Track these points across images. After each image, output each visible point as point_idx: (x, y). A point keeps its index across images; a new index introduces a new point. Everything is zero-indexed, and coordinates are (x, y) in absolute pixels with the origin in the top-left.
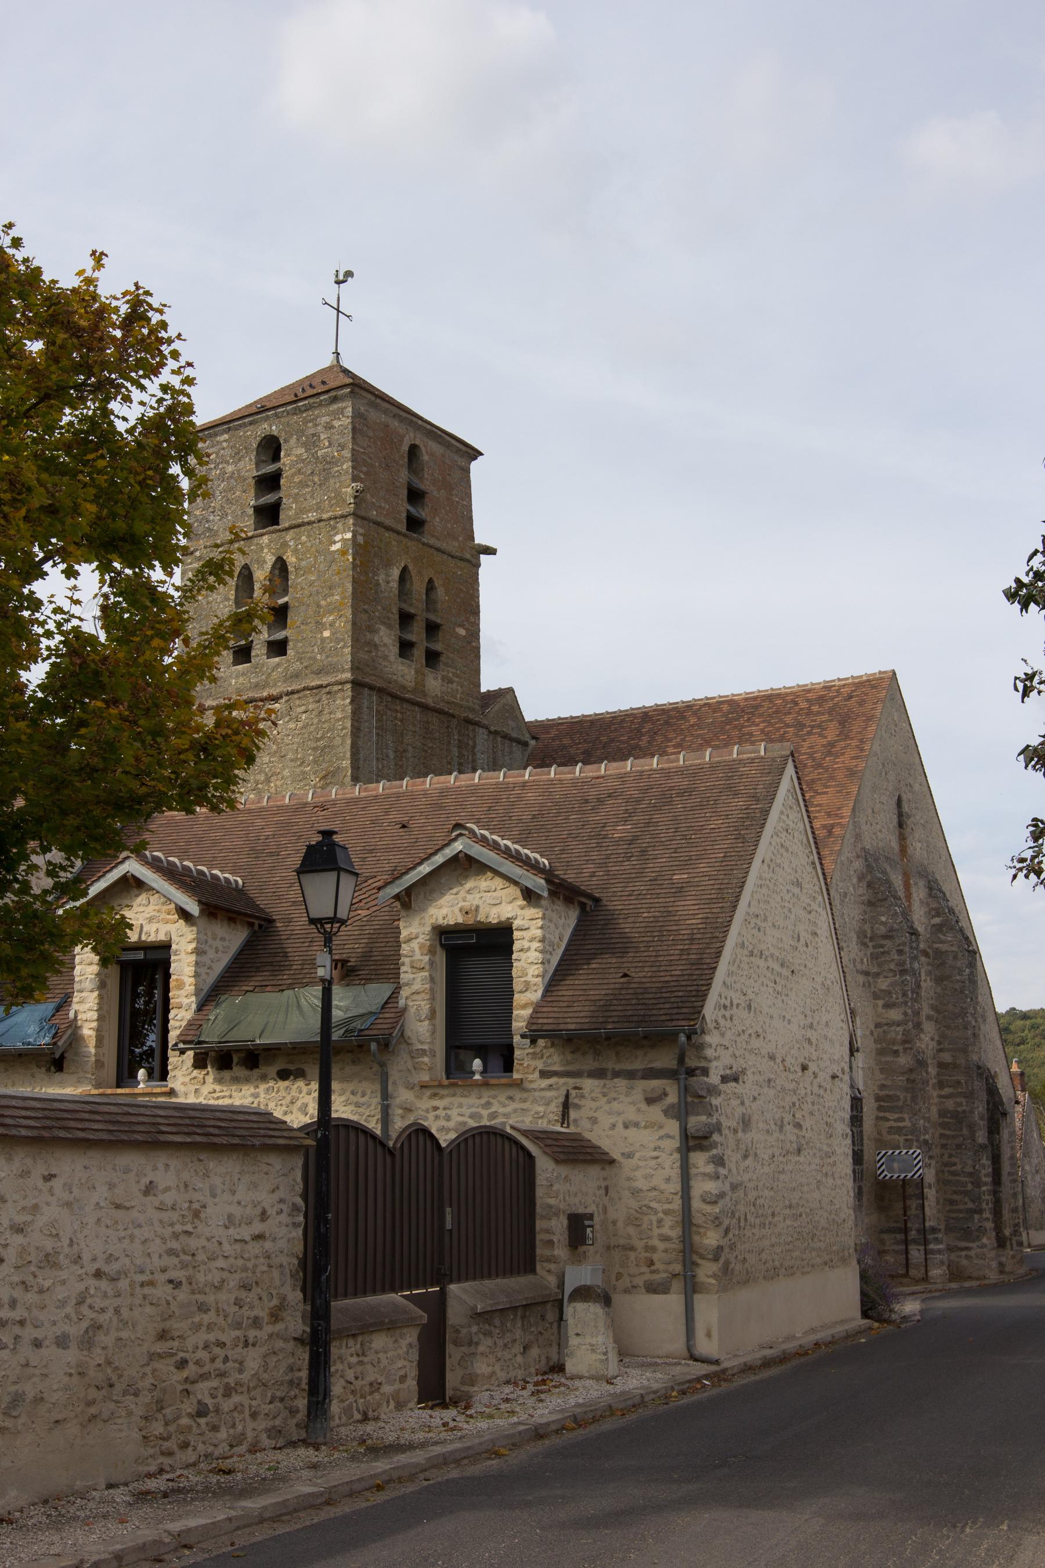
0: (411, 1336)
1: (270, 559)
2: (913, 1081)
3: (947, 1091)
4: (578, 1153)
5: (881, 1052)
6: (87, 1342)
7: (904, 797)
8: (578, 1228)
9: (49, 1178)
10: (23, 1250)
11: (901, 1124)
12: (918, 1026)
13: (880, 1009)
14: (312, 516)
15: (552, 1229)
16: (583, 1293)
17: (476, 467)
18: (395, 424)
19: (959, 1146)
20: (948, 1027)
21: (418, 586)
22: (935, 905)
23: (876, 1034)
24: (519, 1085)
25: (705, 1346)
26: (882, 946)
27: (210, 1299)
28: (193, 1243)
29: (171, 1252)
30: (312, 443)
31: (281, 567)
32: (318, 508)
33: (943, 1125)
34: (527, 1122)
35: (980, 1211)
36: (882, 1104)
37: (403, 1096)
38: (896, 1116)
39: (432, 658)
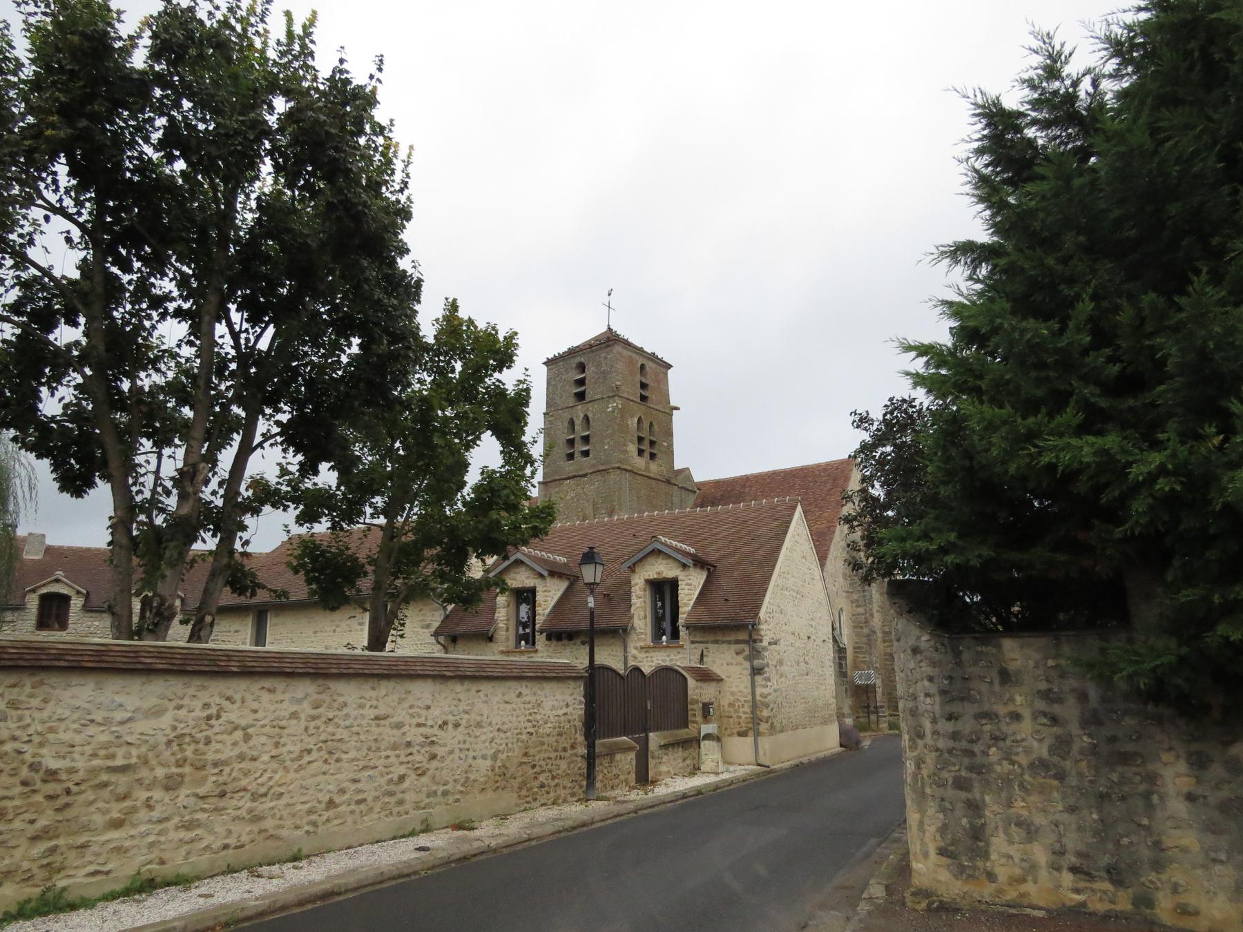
0: (632, 755)
1: (582, 416)
4: (706, 676)
5: (855, 627)
6: (494, 757)
8: (706, 708)
9: (478, 691)
10: (468, 721)
12: (872, 615)
14: (599, 396)
15: (695, 710)
16: (708, 737)
18: (634, 355)
21: (646, 425)
24: (682, 647)
25: (763, 760)
27: (546, 740)
28: (538, 717)
29: (529, 721)
30: (598, 365)
31: (586, 418)
32: (602, 393)
34: (686, 663)
37: (632, 651)
39: (653, 456)
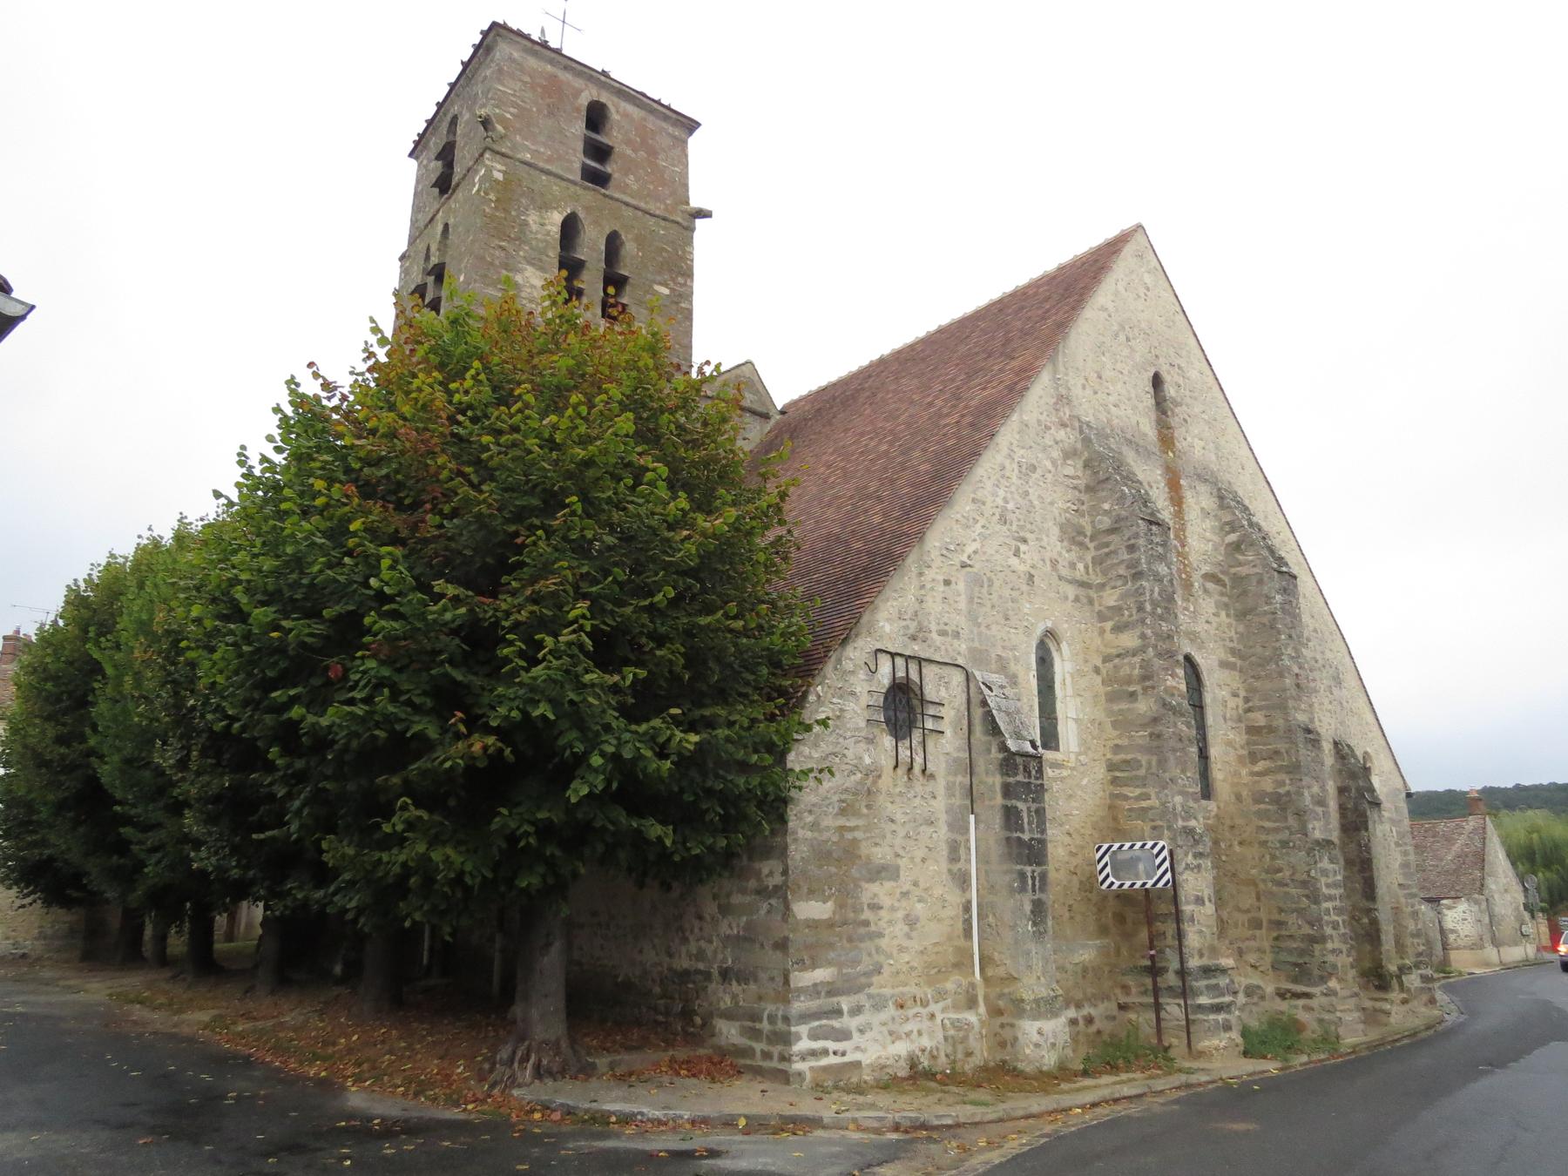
2: (1159, 736)
3: (1261, 766)
5: (1112, 698)
7: (1166, 377)
11: (1144, 804)
13: (1109, 636)
17: (694, 142)
19: (1284, 844)
20: (1257, 678)
22: (1228, 518)
23: (1104, 672)
26: (1107, 545)
33: (1262, 815)
35: (1323, 939)
36: (1118, 774)
38: (1138, 791)
